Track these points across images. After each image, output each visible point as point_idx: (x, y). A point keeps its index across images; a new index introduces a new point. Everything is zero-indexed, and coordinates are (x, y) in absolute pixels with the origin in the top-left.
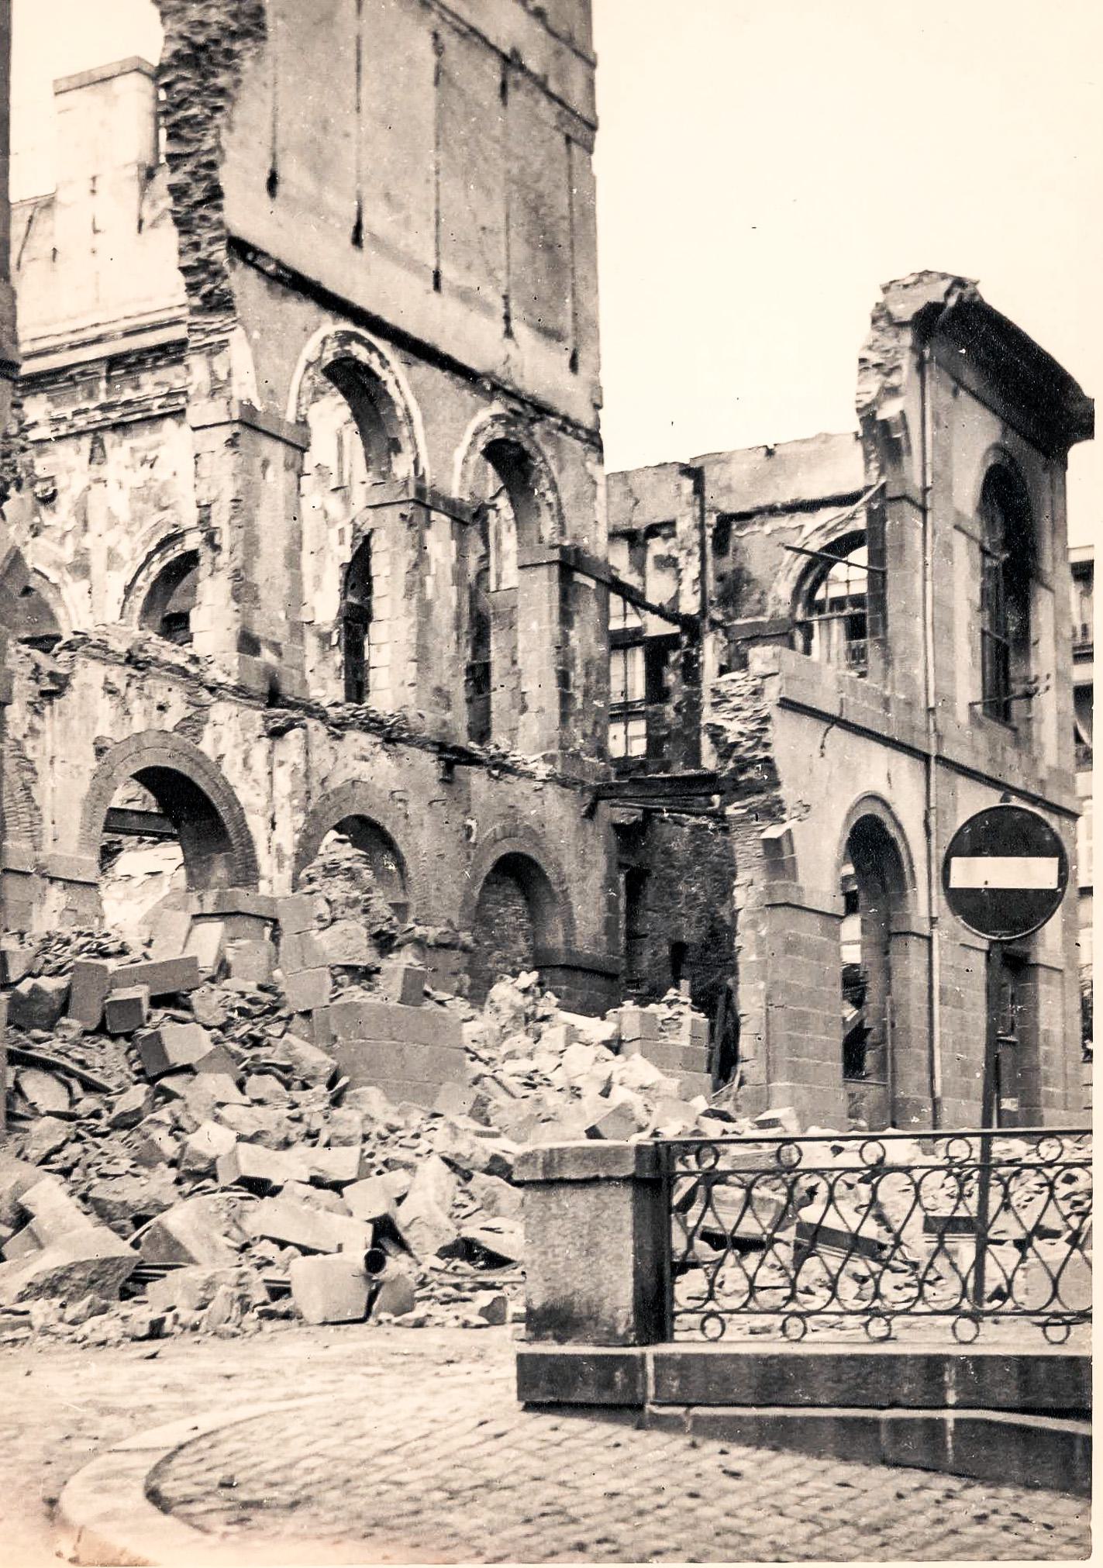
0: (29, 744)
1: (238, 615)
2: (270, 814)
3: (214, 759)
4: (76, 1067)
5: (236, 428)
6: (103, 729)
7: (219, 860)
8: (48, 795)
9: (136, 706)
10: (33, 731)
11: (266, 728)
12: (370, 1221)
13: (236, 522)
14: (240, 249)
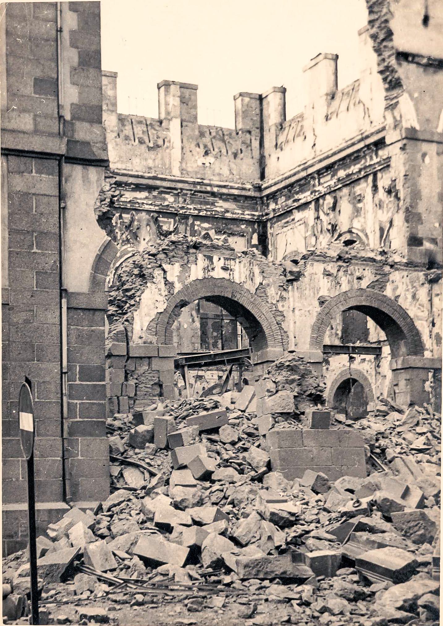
0: (280, 305)
1: (408, 229)
2: (431, 319)
3: (393, 298)
4: (146, 466)
5: (405, 141)
6: (324, 292)
7: (402, 343)
8: (292, 325)
9: (344, 280)
10: (282, 298)
11: (426, 279)
12: (189, 547)
13: (407, 185)
14: (403, 56)
